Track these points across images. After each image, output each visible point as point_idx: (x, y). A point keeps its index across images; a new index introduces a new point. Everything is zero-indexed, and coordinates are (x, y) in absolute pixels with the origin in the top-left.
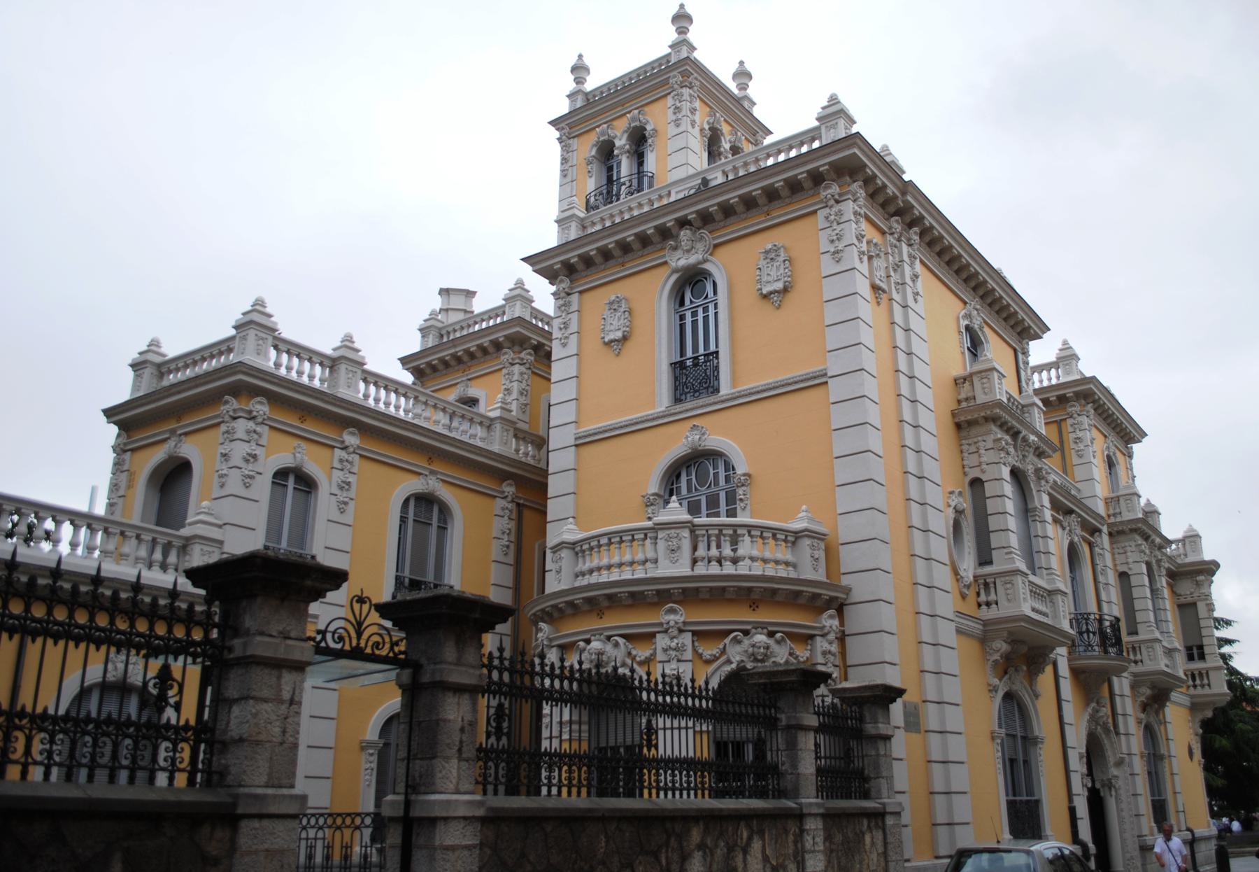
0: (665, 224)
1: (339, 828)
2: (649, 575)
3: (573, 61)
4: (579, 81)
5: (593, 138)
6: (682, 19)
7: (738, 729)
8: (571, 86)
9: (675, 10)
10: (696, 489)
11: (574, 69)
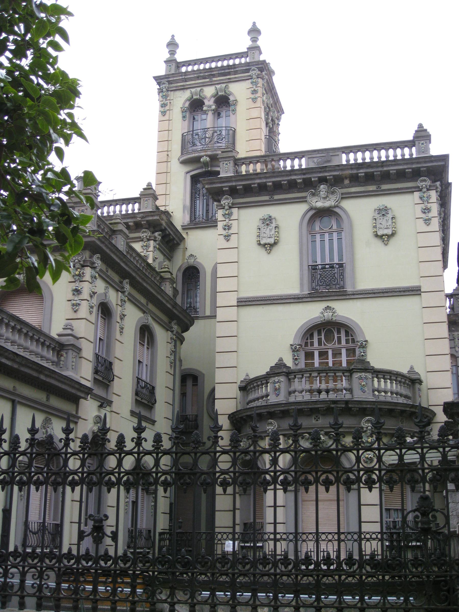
0: (326, 176)
1: (330, 541)
2: (393, 401)
3: (168, 39)
4: (172, 53)
5: (187, 94)
6: (254, 32)
7: (36, 496)
8: (167, 56)
9: (250, 26)
10: (325, 345)
11: (169, 45)
